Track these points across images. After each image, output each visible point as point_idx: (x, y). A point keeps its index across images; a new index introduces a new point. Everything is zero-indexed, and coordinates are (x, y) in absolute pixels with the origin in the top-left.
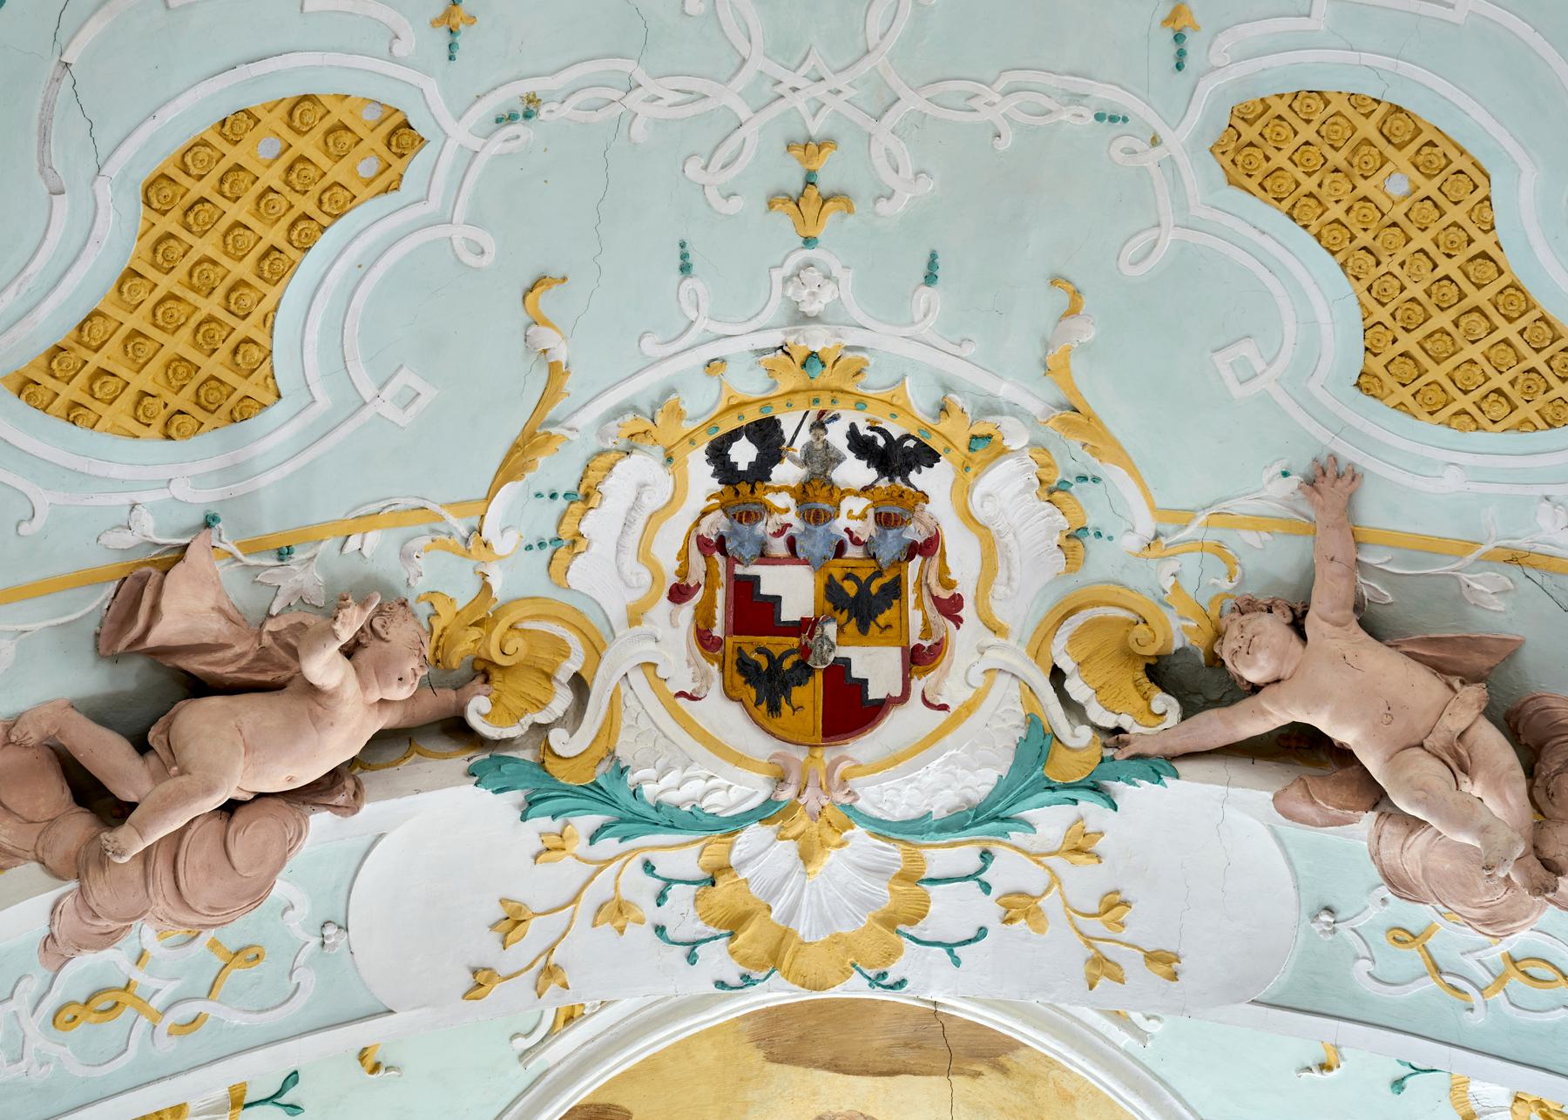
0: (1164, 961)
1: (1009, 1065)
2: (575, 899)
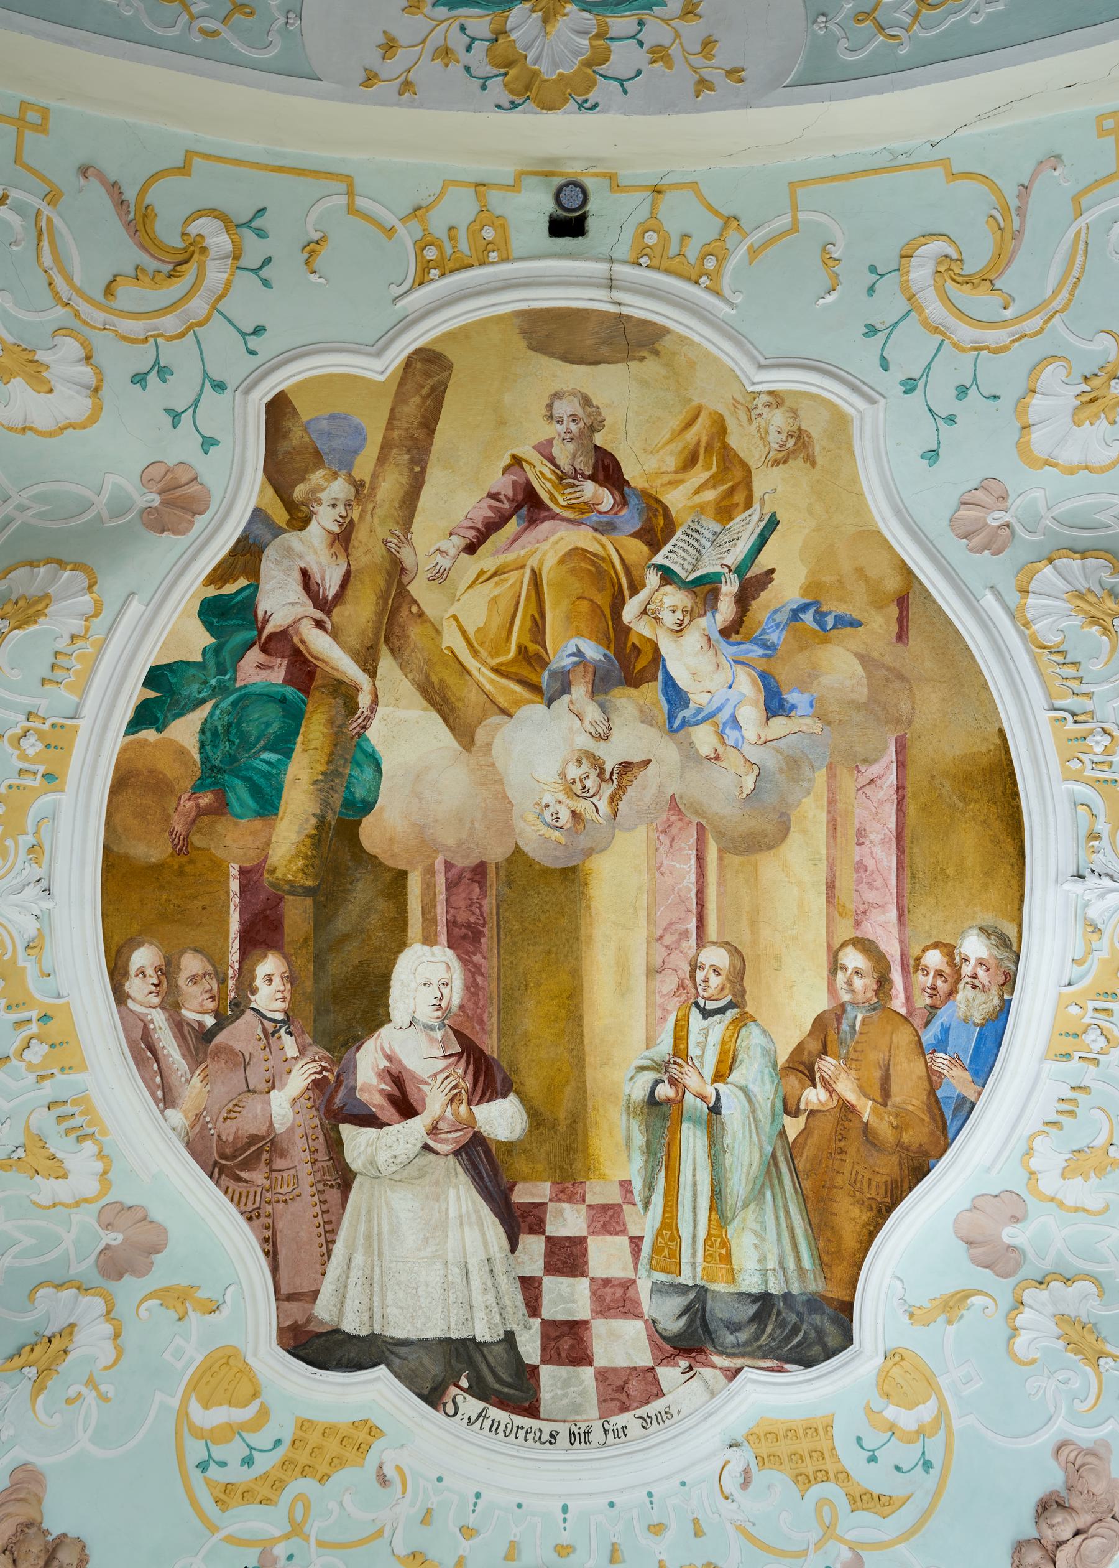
0: (734, 73)
1: (660, 348)
2: (424, 41)
